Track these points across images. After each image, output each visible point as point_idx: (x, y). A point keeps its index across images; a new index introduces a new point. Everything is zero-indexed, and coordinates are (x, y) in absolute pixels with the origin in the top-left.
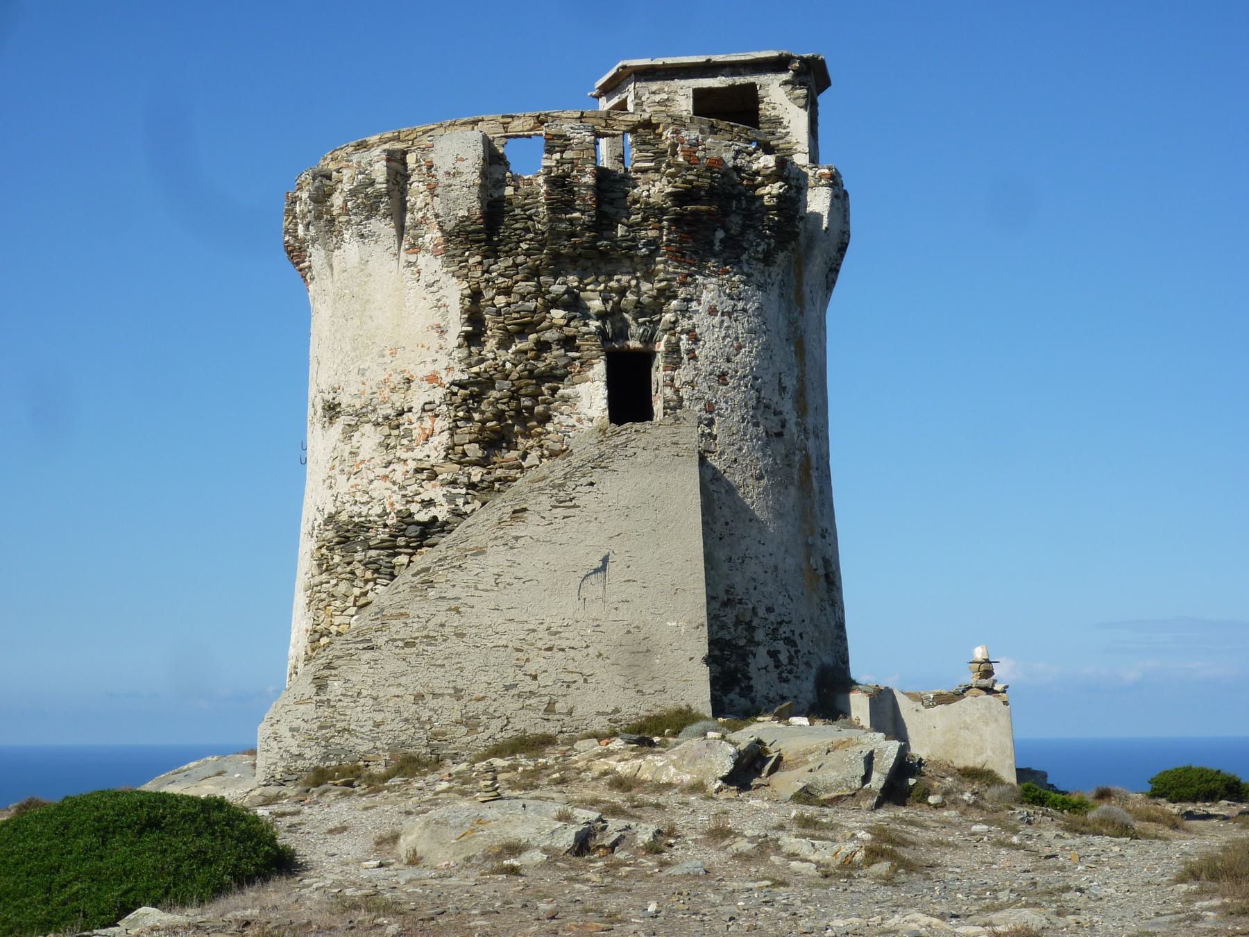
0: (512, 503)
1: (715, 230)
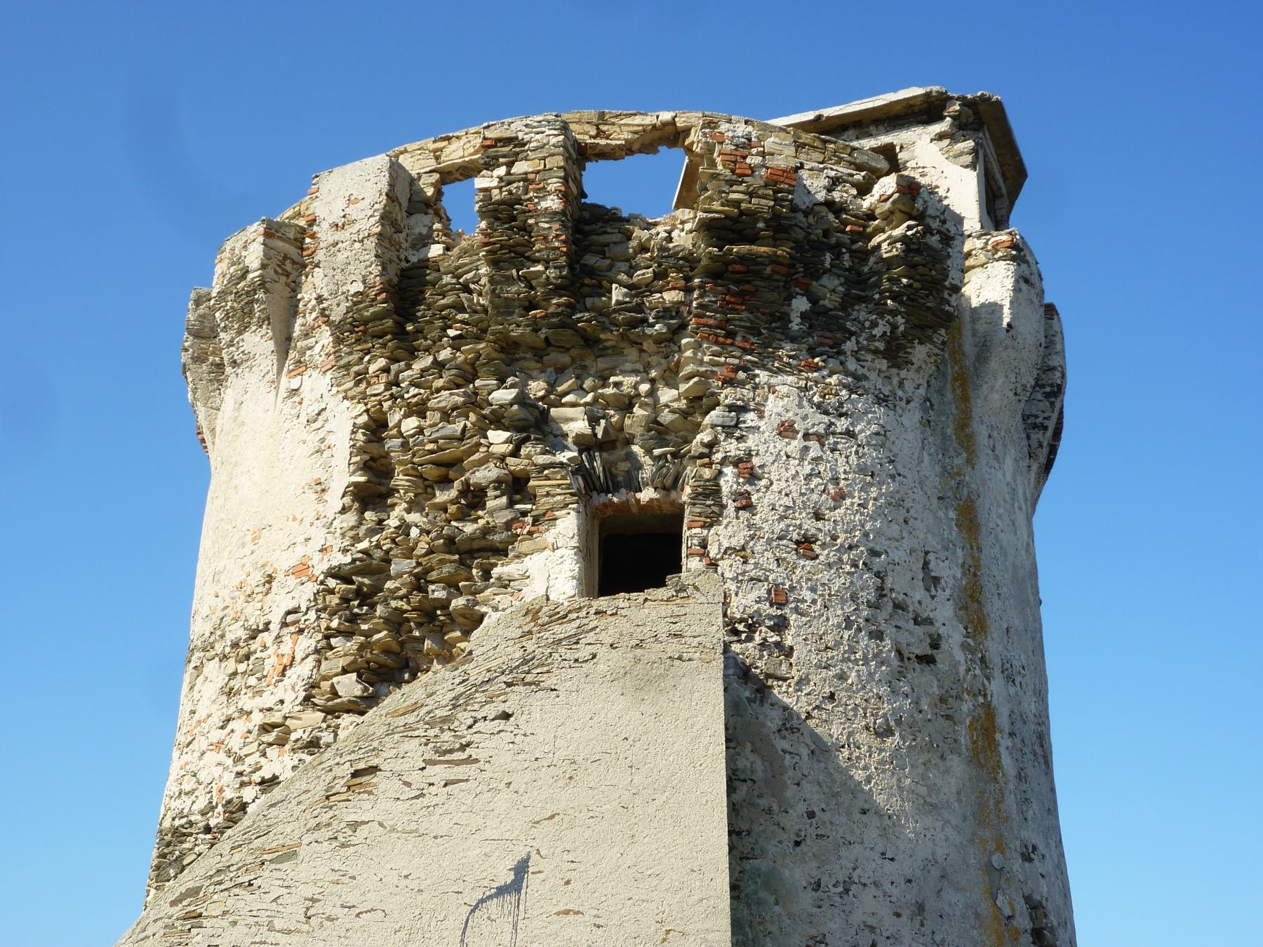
0: (353, 757)
1: (790, 298)
